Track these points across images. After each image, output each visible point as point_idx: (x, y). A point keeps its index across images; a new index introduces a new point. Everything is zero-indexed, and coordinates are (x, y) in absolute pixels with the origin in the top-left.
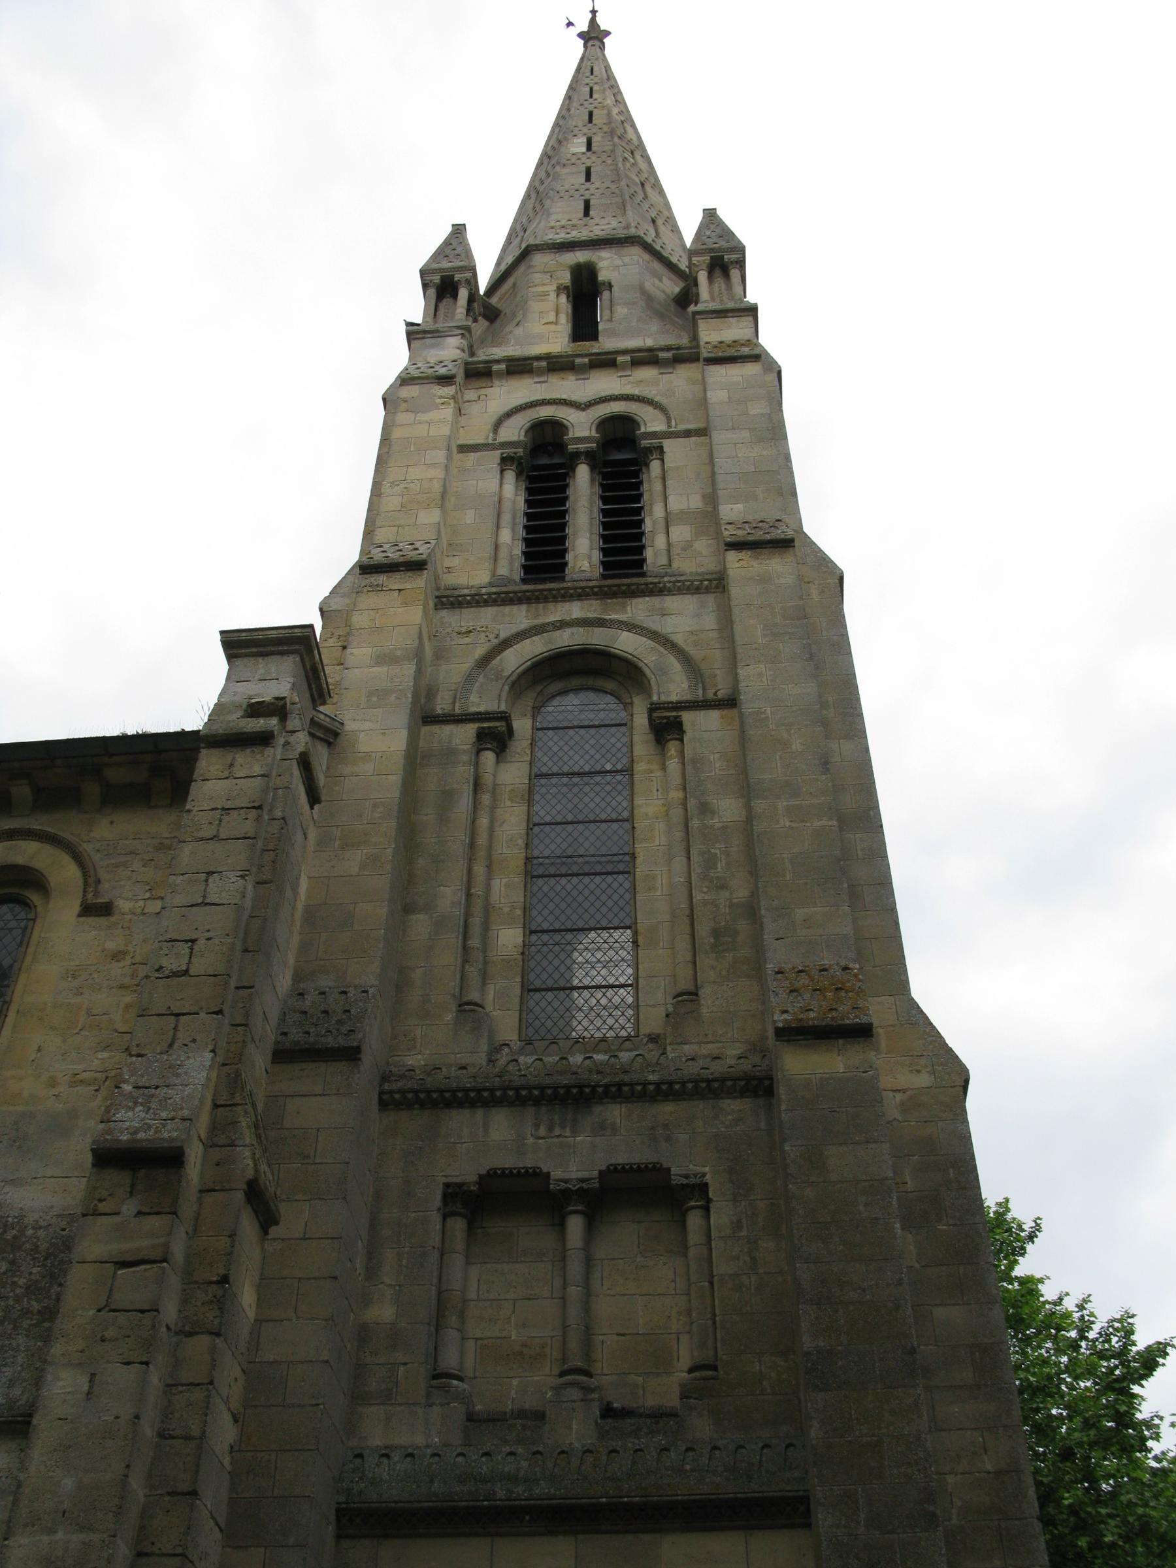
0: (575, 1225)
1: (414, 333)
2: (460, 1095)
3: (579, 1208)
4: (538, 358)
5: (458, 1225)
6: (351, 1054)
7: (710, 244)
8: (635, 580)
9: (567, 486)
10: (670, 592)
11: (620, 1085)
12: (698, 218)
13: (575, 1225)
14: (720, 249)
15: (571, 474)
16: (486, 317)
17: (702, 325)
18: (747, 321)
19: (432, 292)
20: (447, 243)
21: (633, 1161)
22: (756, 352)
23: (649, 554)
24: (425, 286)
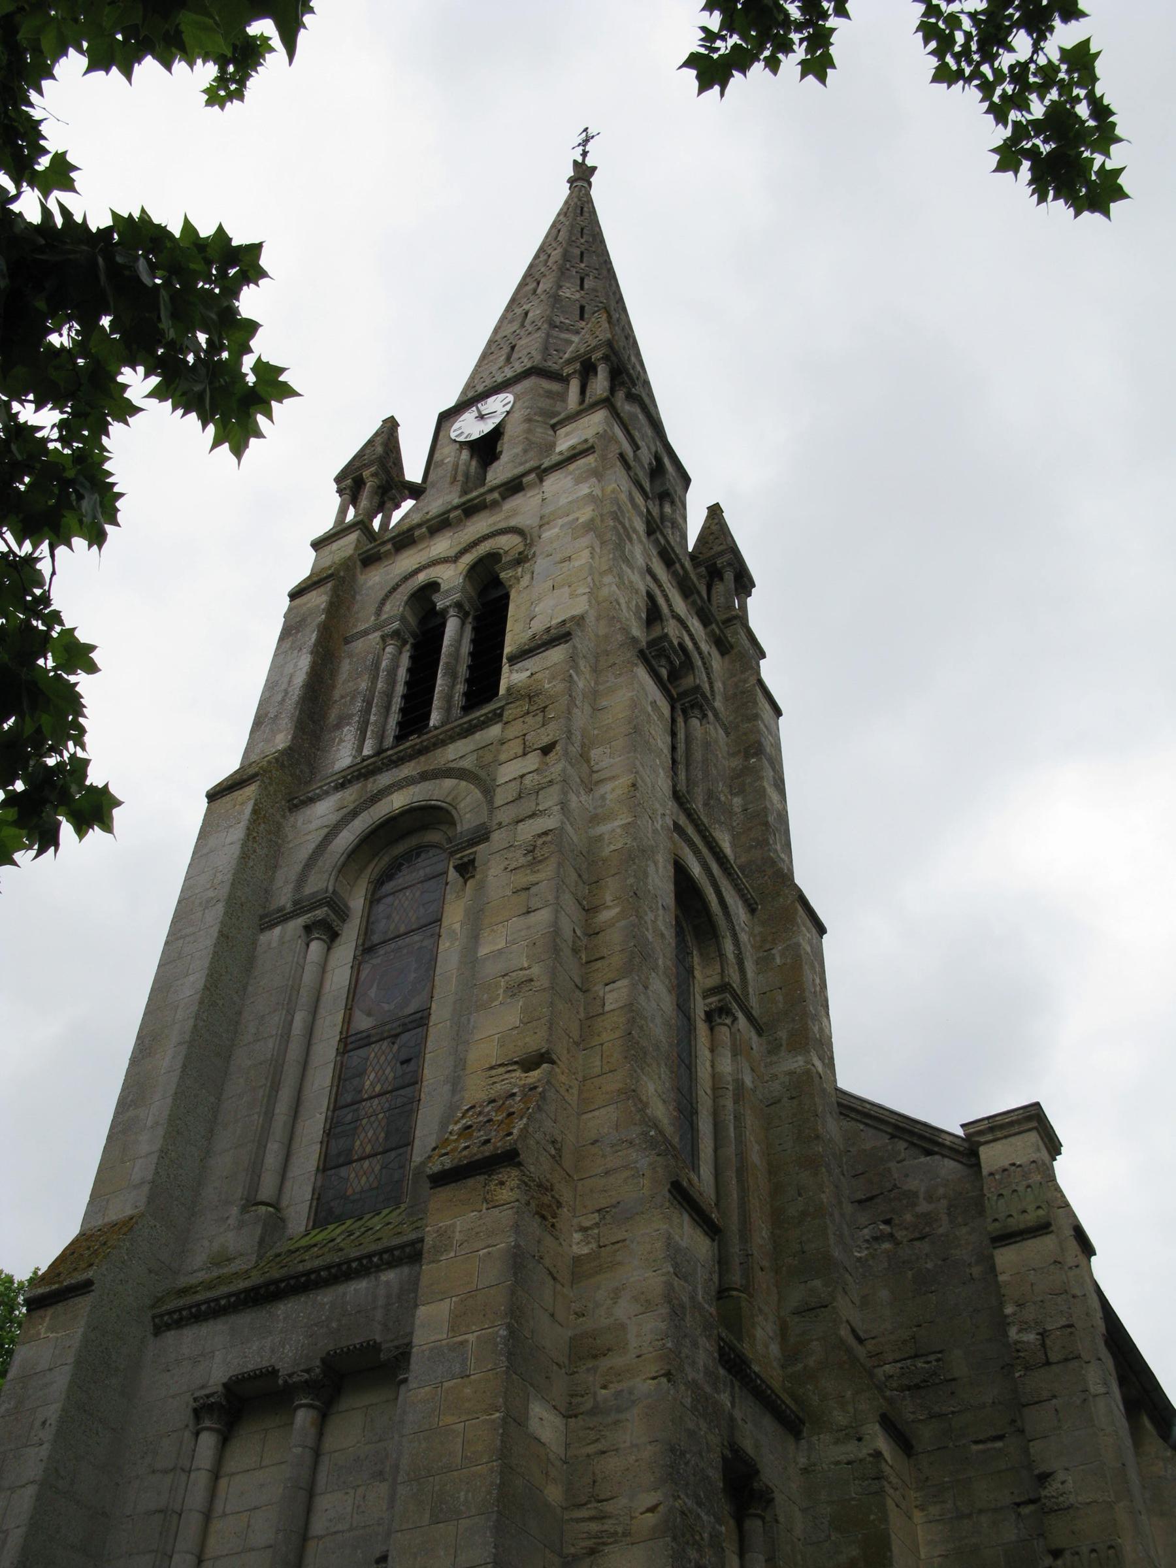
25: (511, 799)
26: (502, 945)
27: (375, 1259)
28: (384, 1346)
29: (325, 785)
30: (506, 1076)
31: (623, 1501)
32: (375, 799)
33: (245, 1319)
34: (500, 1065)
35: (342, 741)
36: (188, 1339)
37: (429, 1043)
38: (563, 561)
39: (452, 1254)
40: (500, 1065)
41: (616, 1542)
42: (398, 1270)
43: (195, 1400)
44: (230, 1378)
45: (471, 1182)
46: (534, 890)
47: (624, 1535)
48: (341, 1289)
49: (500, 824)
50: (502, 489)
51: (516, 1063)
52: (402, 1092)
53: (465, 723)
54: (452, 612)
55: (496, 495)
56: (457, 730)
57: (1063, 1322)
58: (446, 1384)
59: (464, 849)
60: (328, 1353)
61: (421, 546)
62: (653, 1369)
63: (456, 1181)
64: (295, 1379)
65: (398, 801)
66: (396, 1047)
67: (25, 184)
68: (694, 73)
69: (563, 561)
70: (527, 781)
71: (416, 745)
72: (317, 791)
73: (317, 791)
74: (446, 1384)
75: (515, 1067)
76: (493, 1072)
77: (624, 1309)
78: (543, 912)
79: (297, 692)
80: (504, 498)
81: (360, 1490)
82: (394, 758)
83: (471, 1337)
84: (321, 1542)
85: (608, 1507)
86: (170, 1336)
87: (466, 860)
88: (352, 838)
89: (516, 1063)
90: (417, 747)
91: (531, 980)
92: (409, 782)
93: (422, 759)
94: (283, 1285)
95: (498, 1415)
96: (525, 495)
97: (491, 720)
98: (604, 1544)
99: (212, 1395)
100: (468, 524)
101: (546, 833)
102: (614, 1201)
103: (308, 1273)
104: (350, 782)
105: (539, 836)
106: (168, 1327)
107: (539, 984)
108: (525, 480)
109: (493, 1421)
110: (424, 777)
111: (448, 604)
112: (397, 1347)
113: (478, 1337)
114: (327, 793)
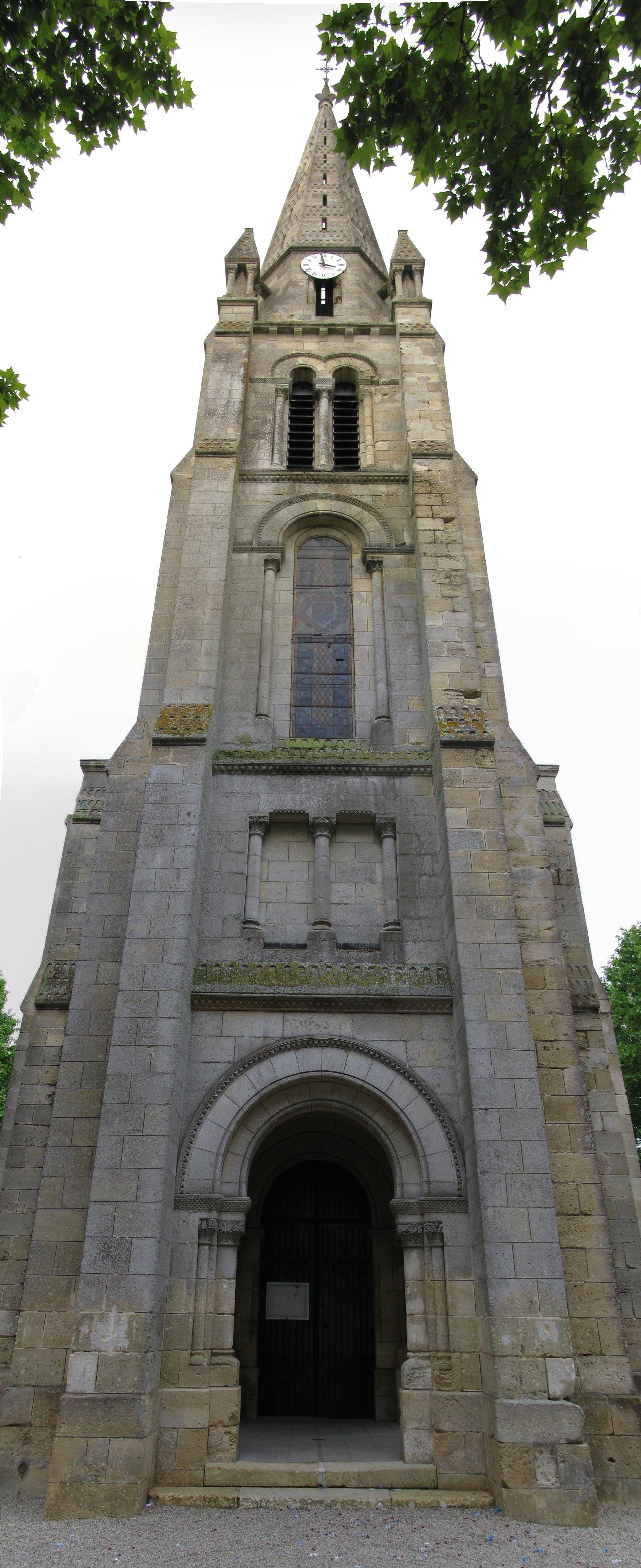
0: (322, 842)
1: (221, 303)
2: (361, 769)
3: (326, 834)
4: (350, 325)
5: (257, 840)
6: (201, 742)
7: (403, 257)
8: (352, 473)
9: (313, 411)
10: (260, 481)
11: (364, 767)
12: (394, 238)
13: (322, 842)
14: (410, 261)
15: (316, 403)
16: (262, 295)
17: (399, 310)
18: (424, 311)
19: (232, 275)
20: (240, 241)
21: (284, 808)
22: (432, 331)
23: (362, 456)
24: (228, 270)
25: (429, 541)
26: (441, 624)
27: (367, 769)
28: (377, 816)
29: (267, 475)
30: (457, 697)
31: (534, 922)
32: (305, 498)
33: (278, 780)
34: (452, 690)
35: (259, 448)
36: (238, 782)
37: (356, 654)
38: (424, 402)
39: (462, 786)
40: (452, 690)
41: (532, 940)
42: (379, 778)
43: (250, 817)
44: (274, 811)
45: (466, 751)
46: (455, 599)
47: (536, 937)
48: (343, 779)
49: (425, 554)
50: (356, 328)
51: (462, 692)
52: (340, 676)
53: (365, 476)
54: (325, 394)
55: (351, 330)
56: (359, 478)
57: (568, 868)
58: (472, 852)
59: (374, 553)
60: (341, 812)
61: (296, 339)
62: (541, 864)
63: (457, 748)
64: (320, 820)
65: (321, 506)
66: (331, 650)
67: (140, 7)
68: (614, 193)
69: (424, 402)
70: (439, 534)
71: (331, 475)
72: (261, 477)
73: (261, 477)
74: (472, 852)
75: (461, 694)
76: (449, 693)
77: (520, 831)
78: (464, 614)
79: (237, 405)
80: (355, 333)
81: (359, 886)
82: (316, 477)
83: (483, 832)
84: (338, 907)
85: (526, 923)
86: (224, 778)
87: (376, 559)
88: (291, 517)
89: (462, 692)
90: (332, 477)
91: (463, 650)
92: (327, 497)
93: (334, 486)
94: (306, 768)
95: (506, 873)
96: (370, 339)
97: (381, 480)
98: (526, 939)
99: (263, 817)
100: (330, 339)
101: (456, 570)
102: (507, 776)
103: (323, 766)
104: (283, 480)
105: (453, 570)
106: (222, 772)
107: (468, 653)
108: (372, 329)
109: (505, 876)
110: (338, 498)
111: (324, 388)
112: (386, 819)
113: (487, 832)
114: (266, 480)
